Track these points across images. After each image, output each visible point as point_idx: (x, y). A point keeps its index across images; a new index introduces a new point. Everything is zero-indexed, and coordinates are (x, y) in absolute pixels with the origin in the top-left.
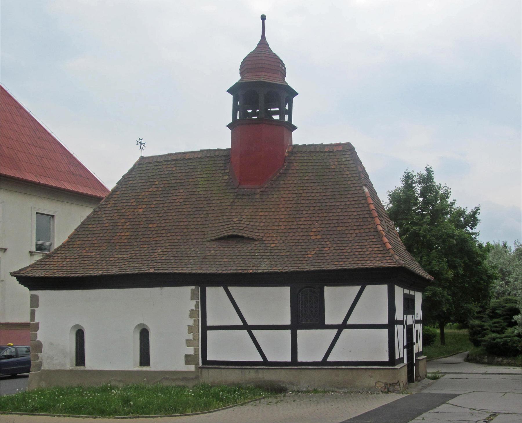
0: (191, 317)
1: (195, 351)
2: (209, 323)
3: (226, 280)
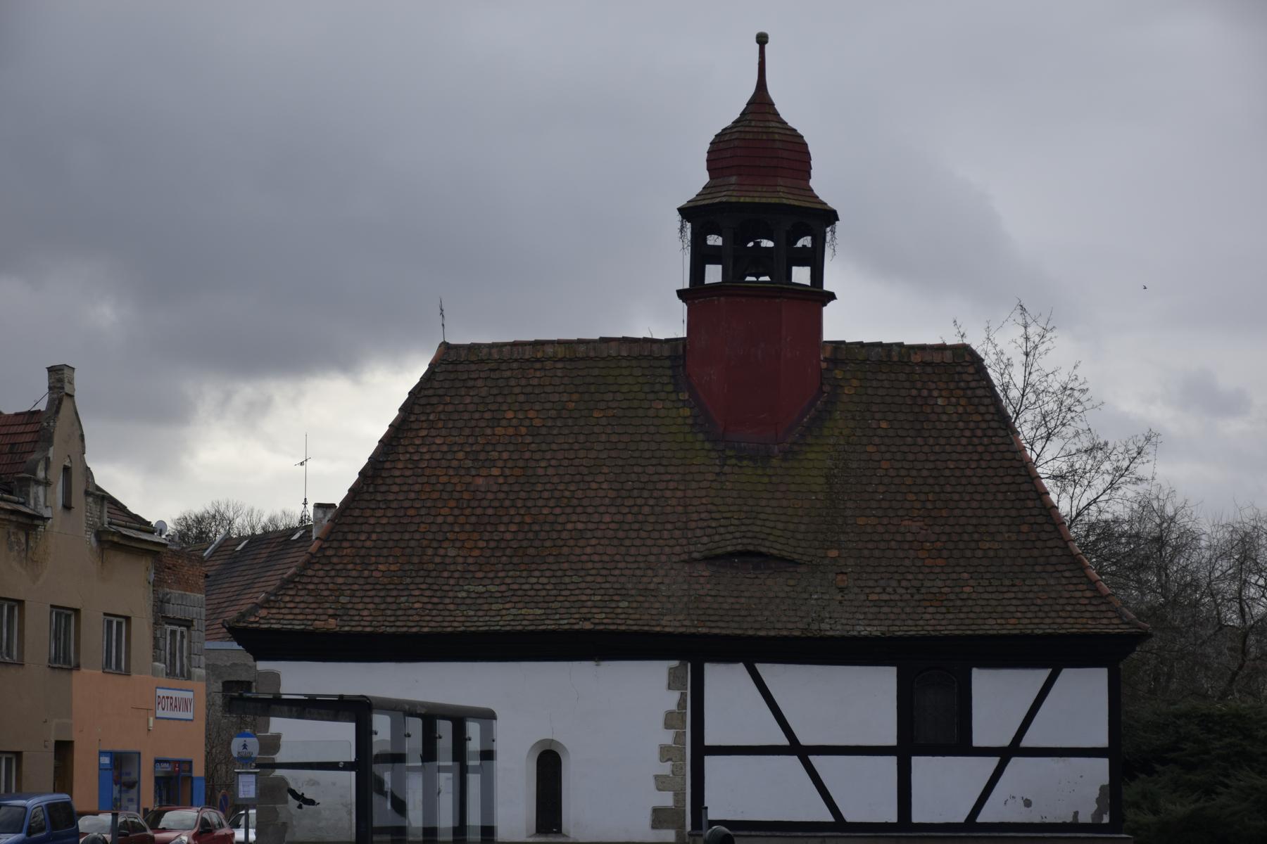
0: (668, 726)
1: (676, 801)
2: (709, 741)
3: (753, 651)
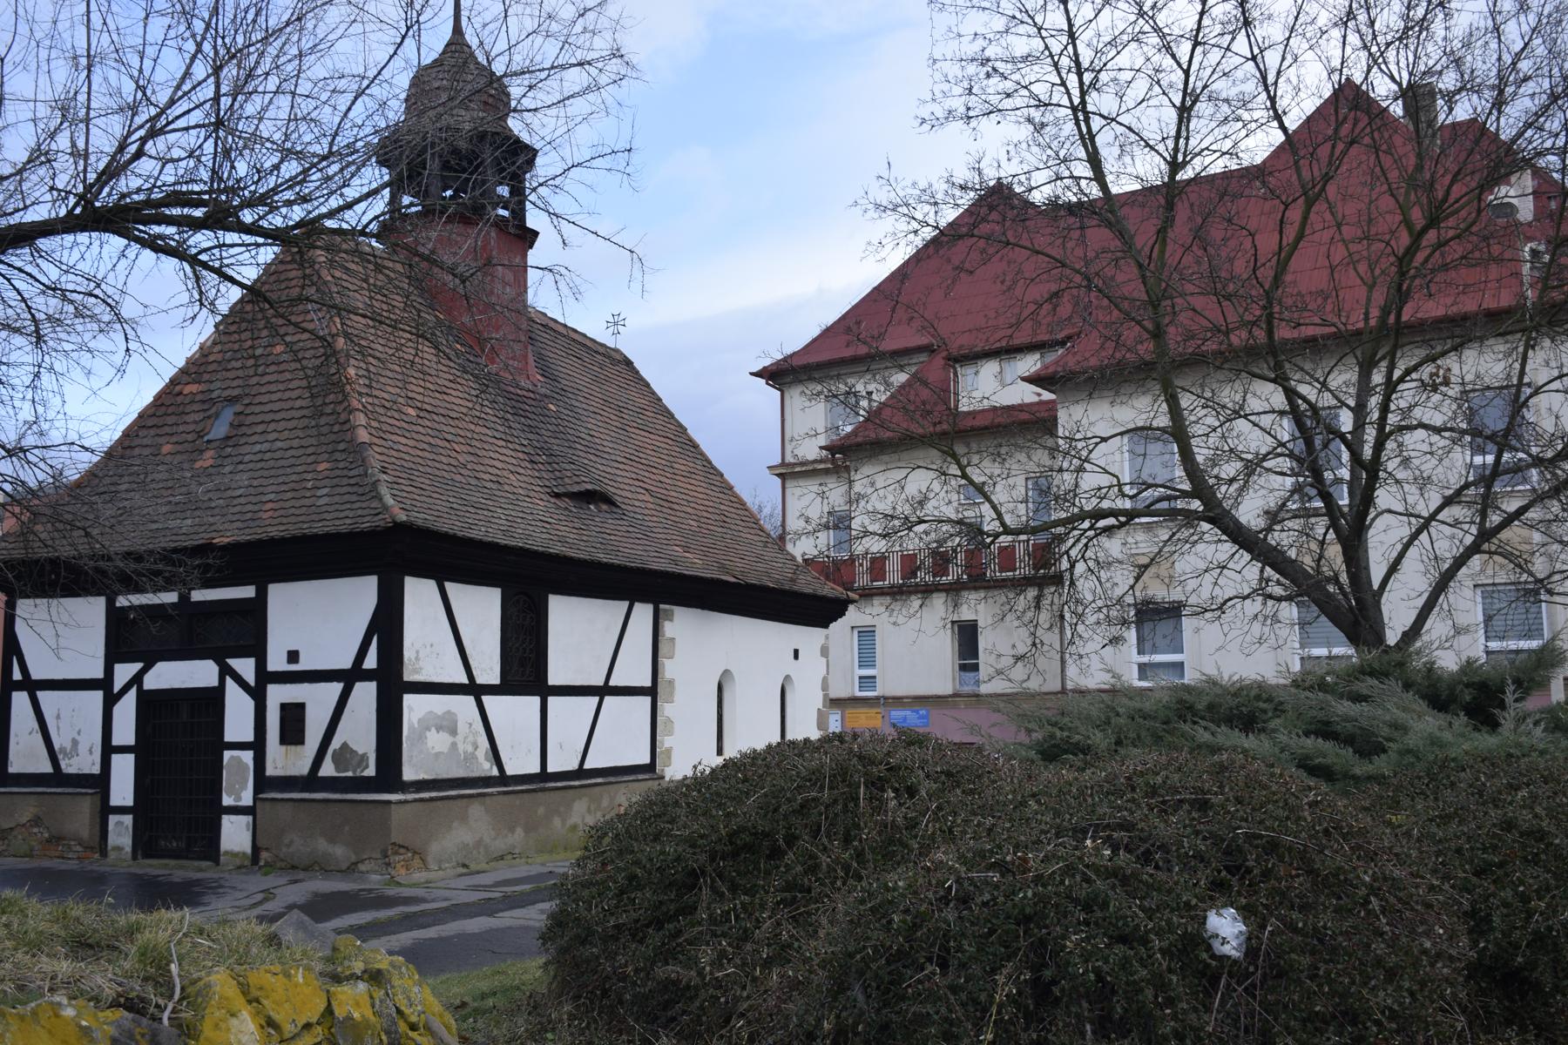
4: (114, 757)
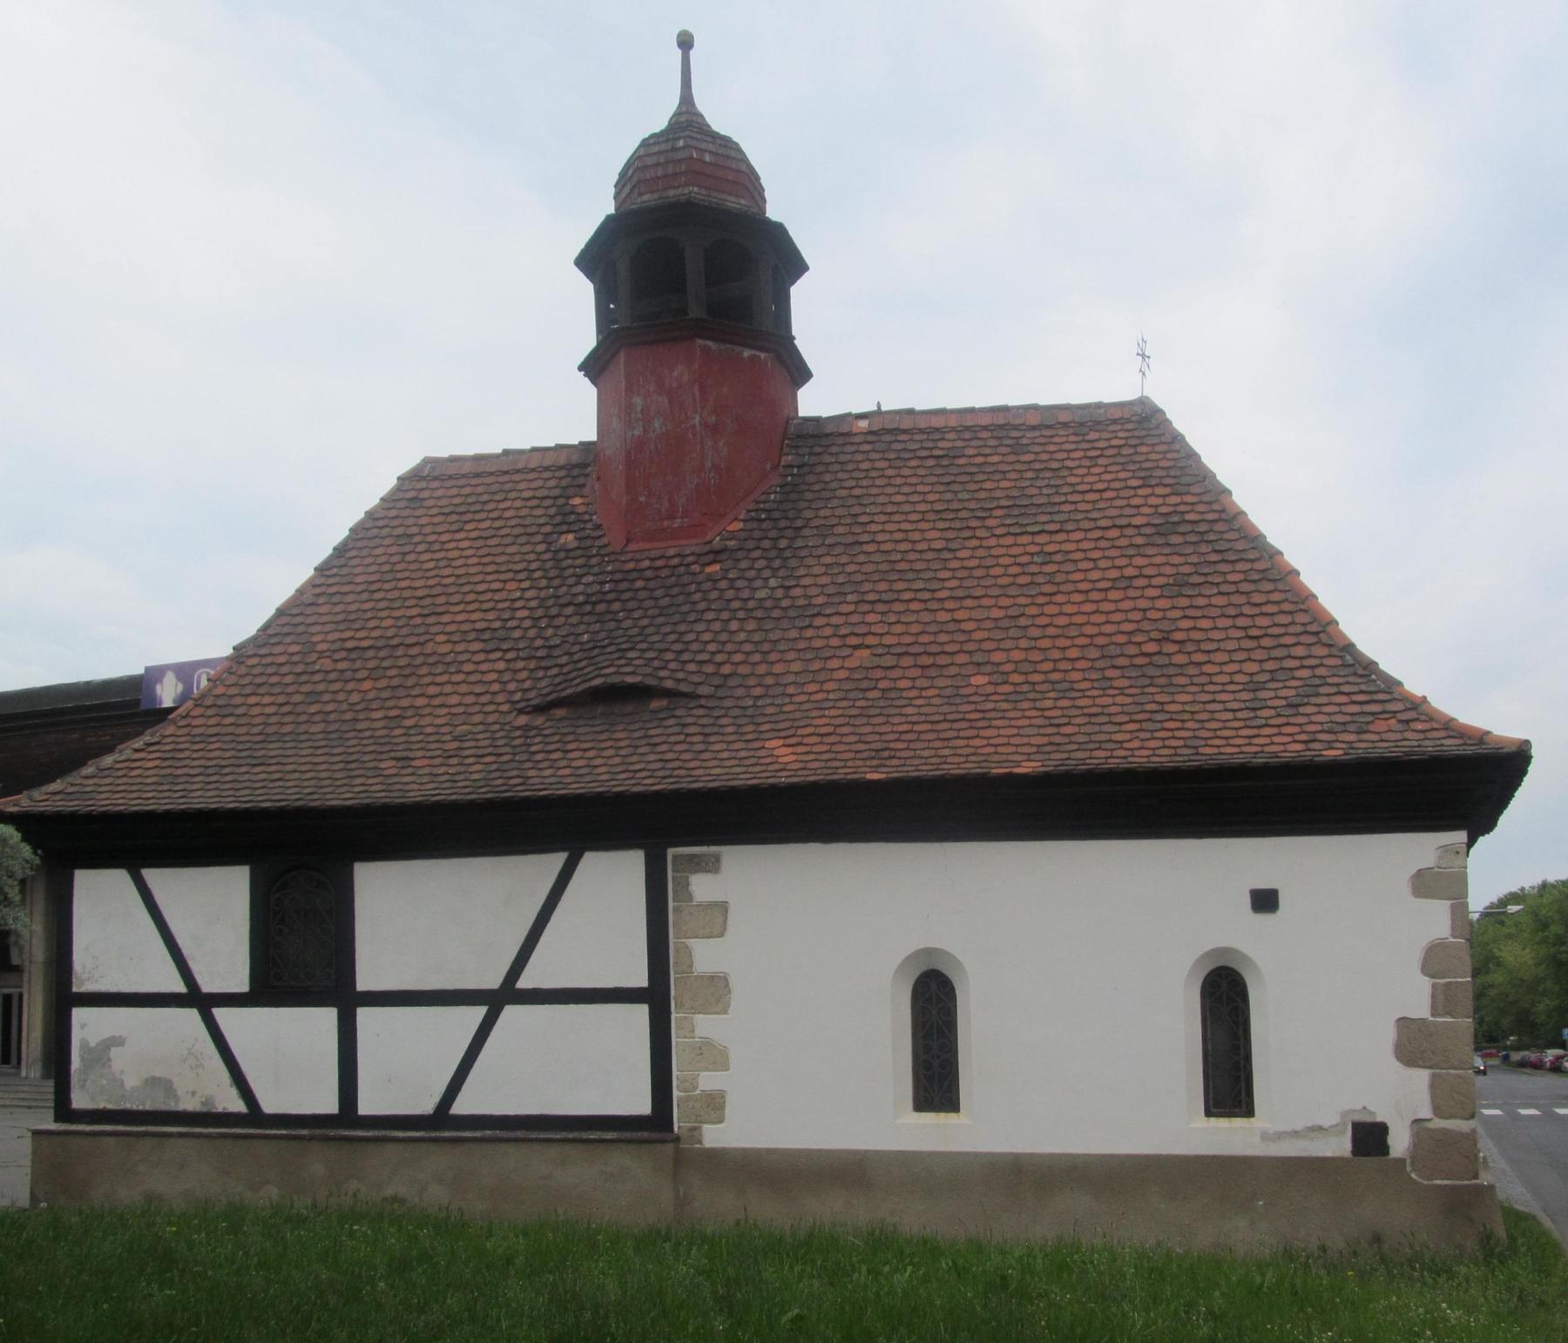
2: (641, 1012)
4: (643, 982)
